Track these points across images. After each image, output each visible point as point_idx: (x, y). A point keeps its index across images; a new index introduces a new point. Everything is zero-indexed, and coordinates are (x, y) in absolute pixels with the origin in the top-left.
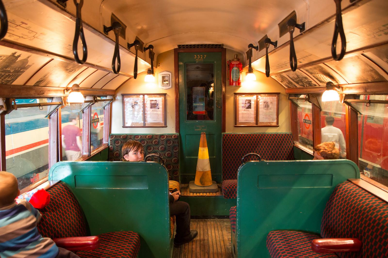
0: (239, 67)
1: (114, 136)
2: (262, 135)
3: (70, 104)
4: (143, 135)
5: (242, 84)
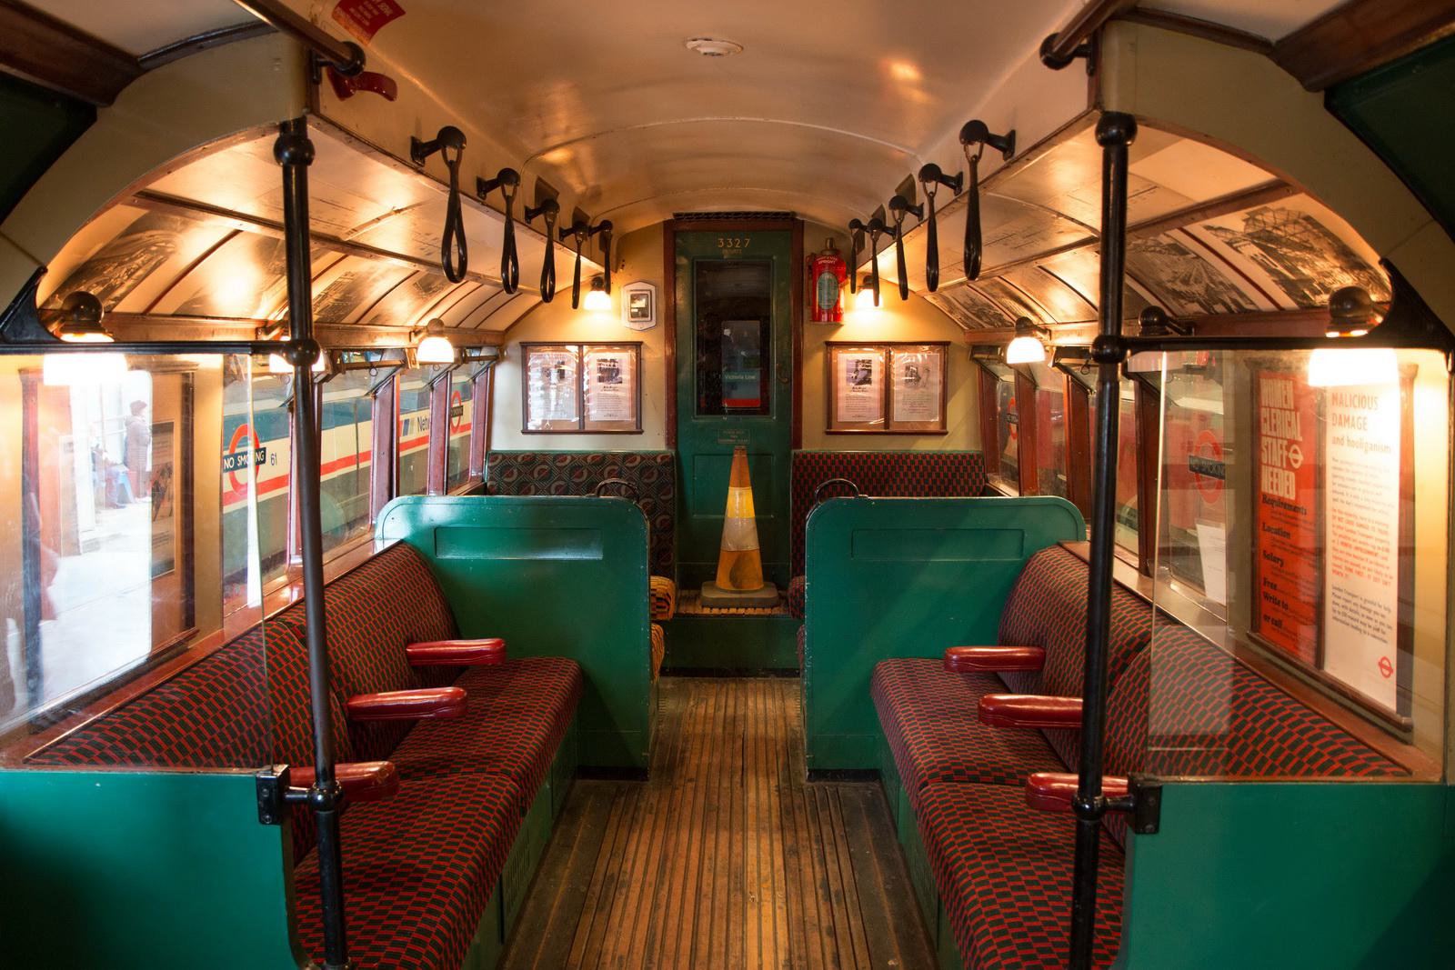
0: (835, 274)
1: (500, 457)
2: (900, 457)
3: (422, 364)
4: (578, 453)
5: (847, 318)
